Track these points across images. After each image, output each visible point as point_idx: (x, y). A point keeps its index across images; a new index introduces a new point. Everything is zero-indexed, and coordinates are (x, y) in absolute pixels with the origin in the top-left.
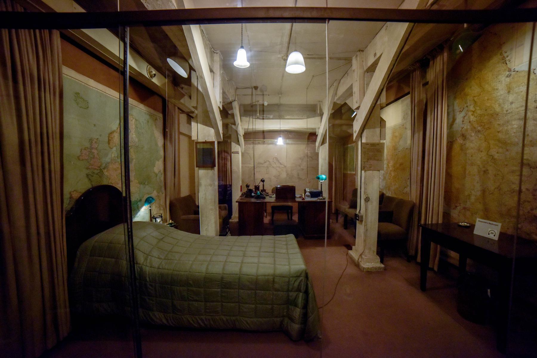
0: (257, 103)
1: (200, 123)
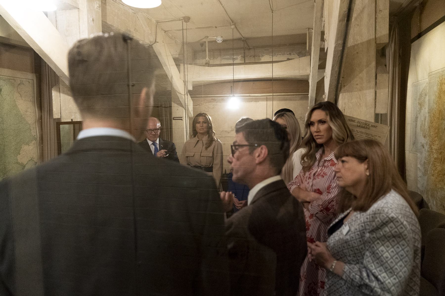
0: (204, 40)
1: (64, 93)
